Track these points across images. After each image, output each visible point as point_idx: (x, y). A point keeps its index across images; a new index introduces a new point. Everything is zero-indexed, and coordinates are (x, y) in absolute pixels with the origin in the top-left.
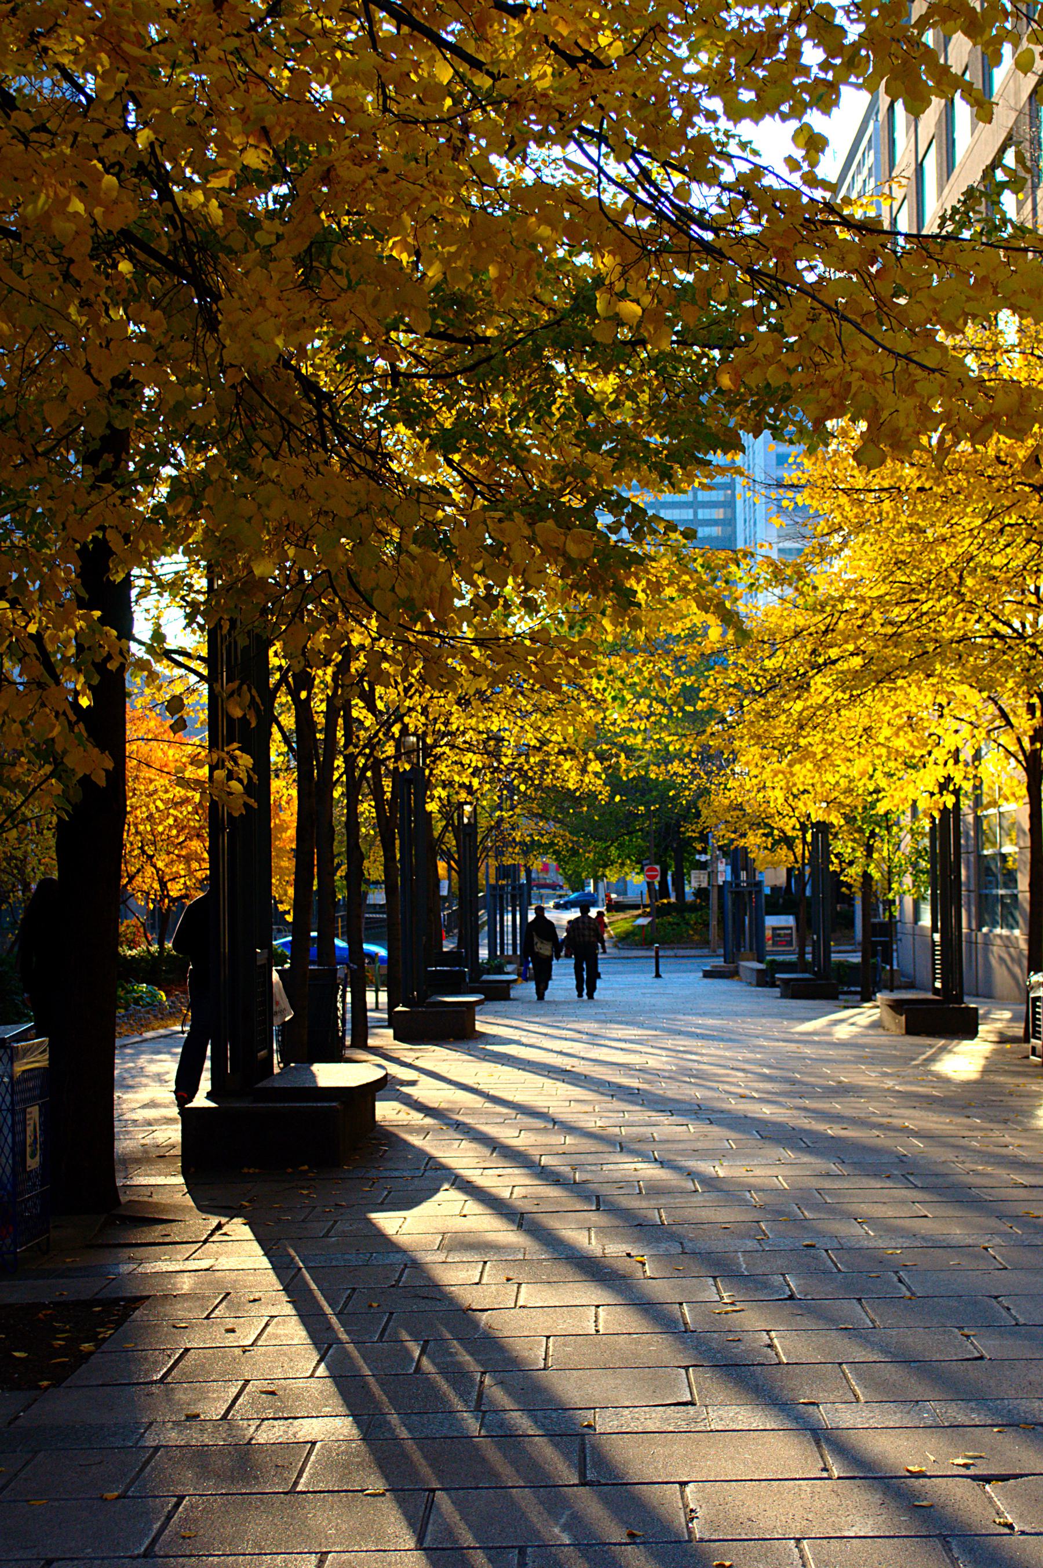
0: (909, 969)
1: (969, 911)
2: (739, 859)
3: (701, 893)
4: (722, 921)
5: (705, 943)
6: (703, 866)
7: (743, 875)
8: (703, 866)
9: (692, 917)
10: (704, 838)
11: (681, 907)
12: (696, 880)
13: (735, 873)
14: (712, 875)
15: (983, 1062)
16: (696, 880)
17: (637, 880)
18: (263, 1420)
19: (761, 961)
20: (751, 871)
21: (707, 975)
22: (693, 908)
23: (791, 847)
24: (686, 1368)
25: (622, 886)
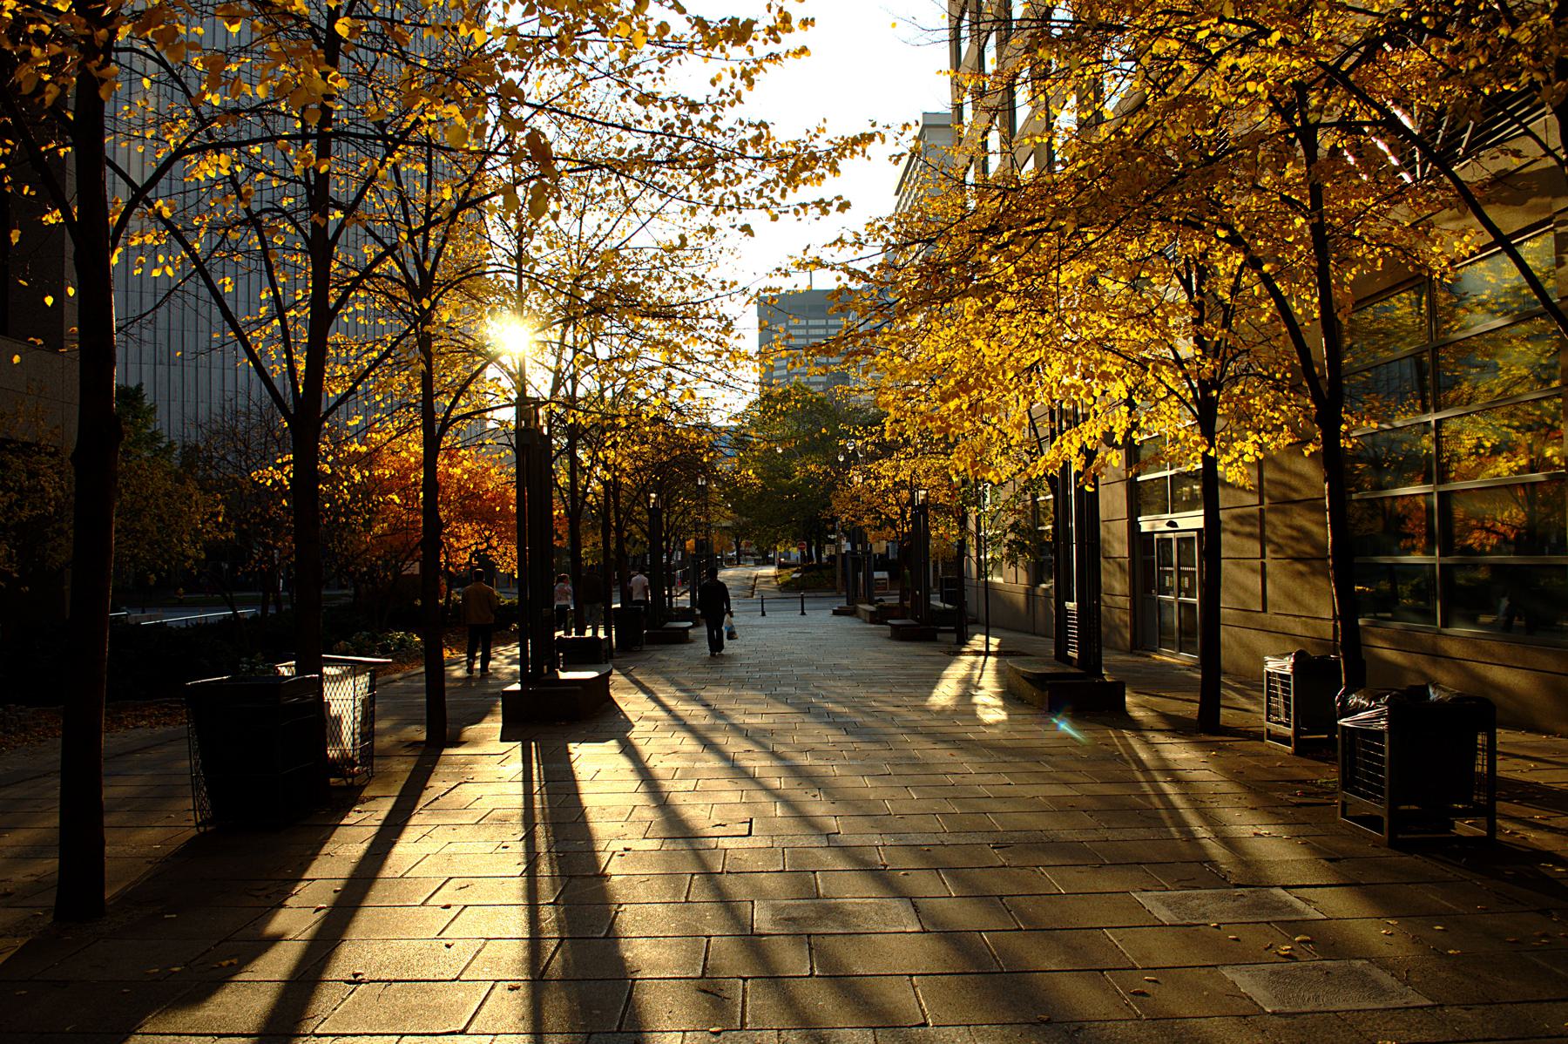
0: (974, 610)
1: (1046, 608)
2: (856, 535)
3: (830, 558)
4: (844, 575)
5: (834, 588)
6: (832, 542)
7: (859, 547)
8: (832, 542)
9: (826, 573)
10: (834, 519)
11: (820, 566)
12: (828, 551)
13: (854, 547)
14: (839, 547)
15: (333, 896)
16: (828, 551)
17: (795, 551)
18: (403, 1035)
19: (871, 604)
20: (864, 543)
21: (835, 613)
22: (826, 567)
23: (894, 526)
24: (745, 979)
25: (787, 555)
